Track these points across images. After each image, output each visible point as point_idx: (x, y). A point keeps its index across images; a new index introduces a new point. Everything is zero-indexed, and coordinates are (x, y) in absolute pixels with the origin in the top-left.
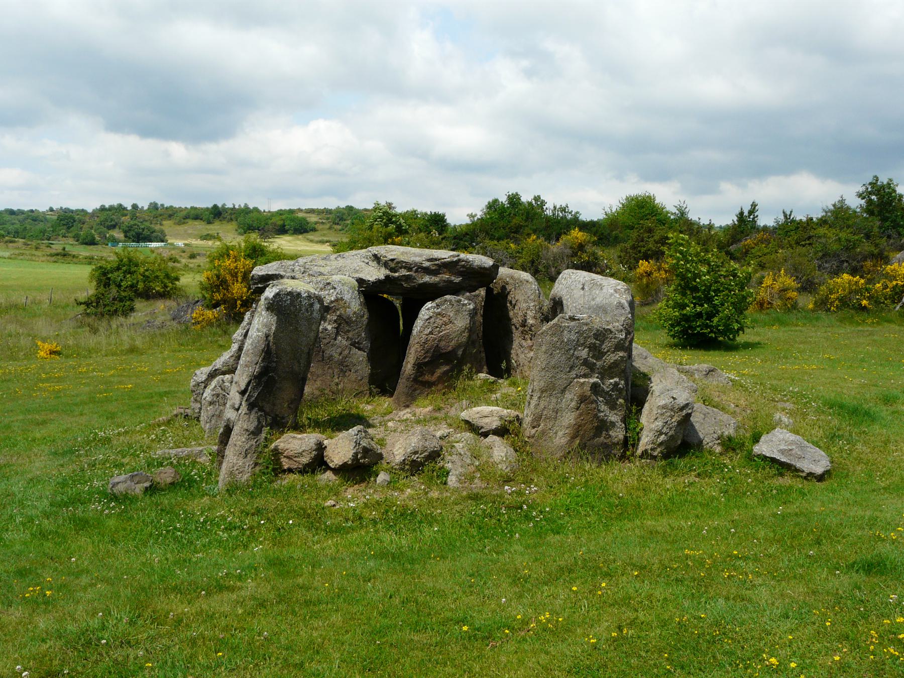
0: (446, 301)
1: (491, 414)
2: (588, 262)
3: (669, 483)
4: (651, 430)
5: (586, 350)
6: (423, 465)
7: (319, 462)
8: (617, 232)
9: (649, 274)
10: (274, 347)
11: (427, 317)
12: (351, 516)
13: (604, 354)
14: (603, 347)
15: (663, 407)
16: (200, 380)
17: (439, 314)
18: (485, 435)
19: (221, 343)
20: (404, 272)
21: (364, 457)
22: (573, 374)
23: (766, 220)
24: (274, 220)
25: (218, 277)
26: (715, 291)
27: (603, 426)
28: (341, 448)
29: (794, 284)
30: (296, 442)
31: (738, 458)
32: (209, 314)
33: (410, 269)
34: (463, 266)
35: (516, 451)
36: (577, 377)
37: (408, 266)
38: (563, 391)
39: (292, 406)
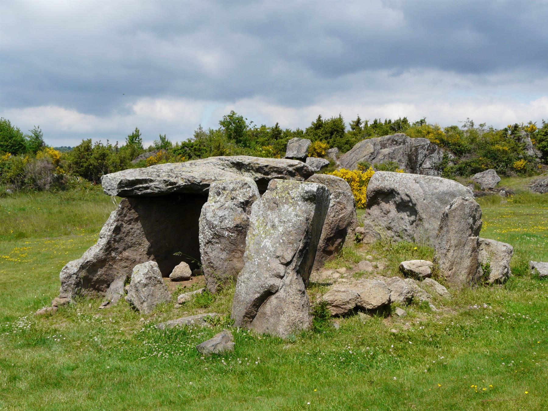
4: (501, 266)
17: (338, 202)
34: (306, 170)
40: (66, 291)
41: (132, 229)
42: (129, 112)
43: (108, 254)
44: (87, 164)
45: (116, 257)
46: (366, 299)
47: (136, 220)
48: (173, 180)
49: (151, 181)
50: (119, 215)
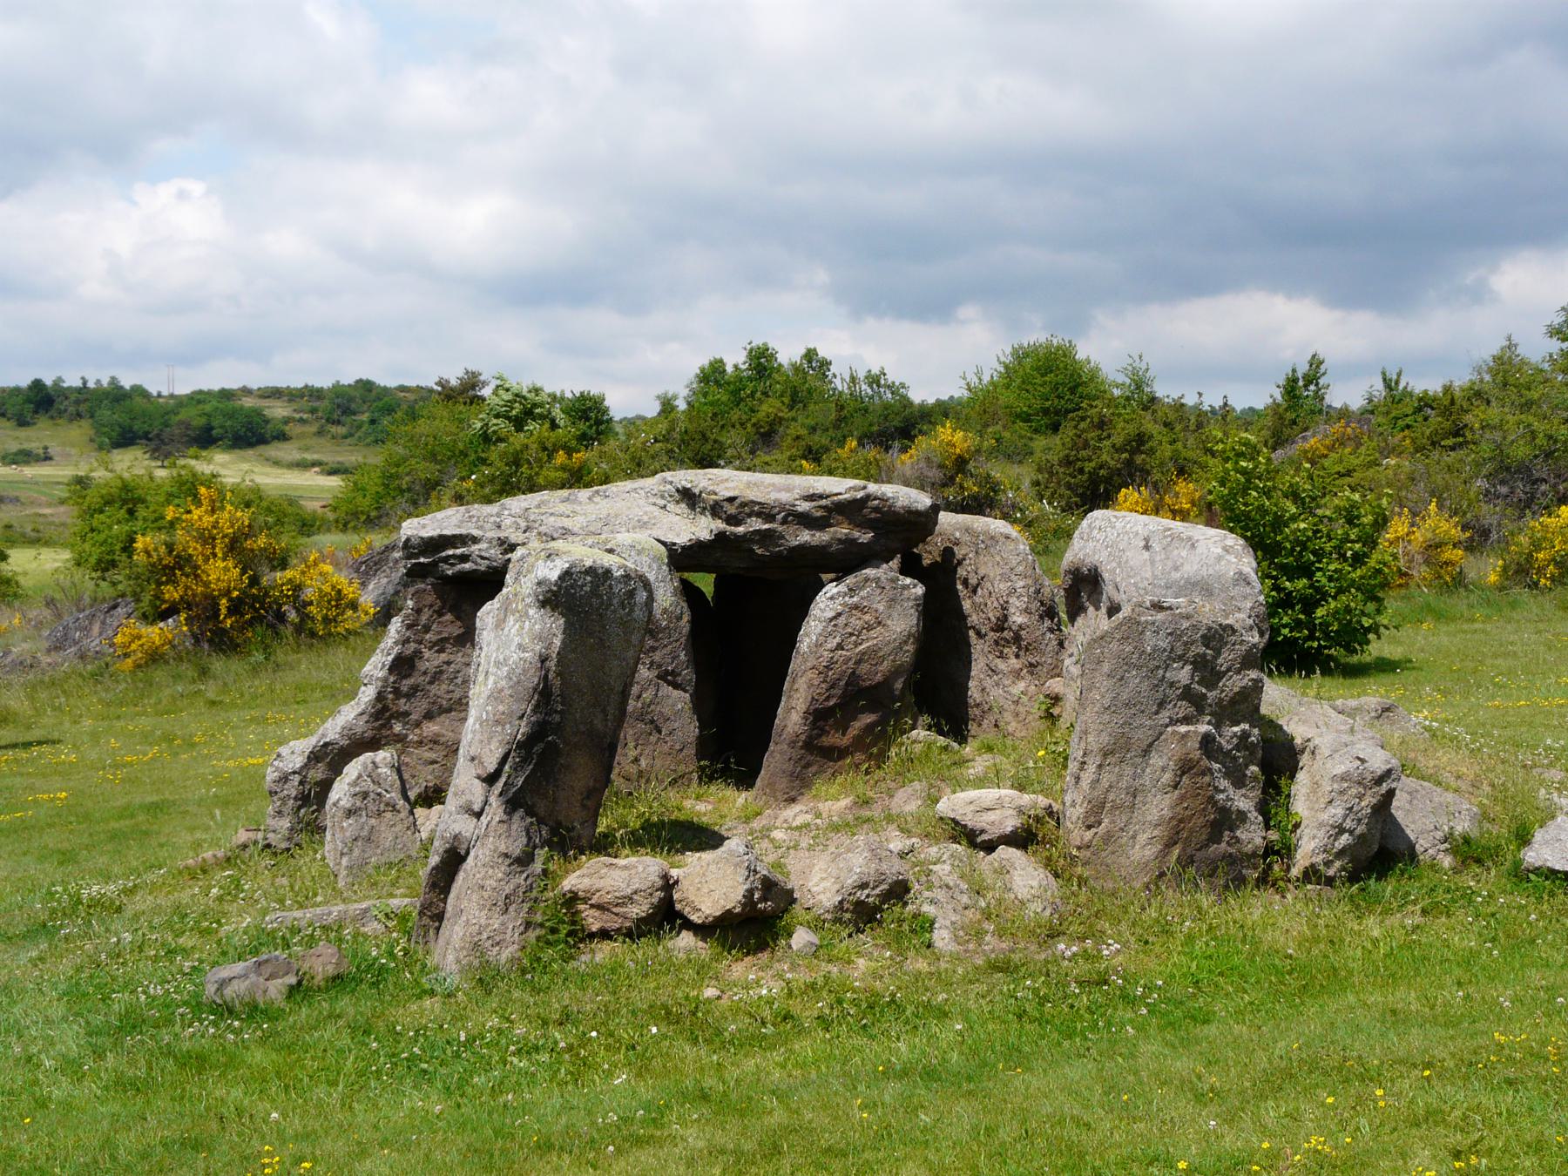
0: (867, 580)
1: (1000, 804)
2: (975, 498)
3: (1373, 926)
4: (1321, 825)
5: (1188, 668)
6: (875, 908)
7: (666, 914)
10: (557, 683)
11: (832, 614)
12: (767, 1013)
14: (1220, 661)
15: (1344, 778)
16: (289, 767)
17: (856, 607)
18: (990, 847)
19: (211, 695)
20: (756, 524)
21: (764, 899)
22: (1164, 716)
23: (1347, 393)
24: (183, 415)
25: (170, 547)
26: (1314, 553)
27: (1226, 820)
28: (711, 884)
29: (1456, 533)
30: (616, 874)
32: (155, 633)
33: (770, 518)
34: (876, 509)
35: (1056, 876)
36: (1173, 722)
38: (1146, 752)
39: (589, 803)
40: (279, 812)
41: (448, 663)
42: (1479, 295)
43: (383, 726)
44: (1093, 464)
45: (406, 736)
49: (475, 540)
50: (409, 627)
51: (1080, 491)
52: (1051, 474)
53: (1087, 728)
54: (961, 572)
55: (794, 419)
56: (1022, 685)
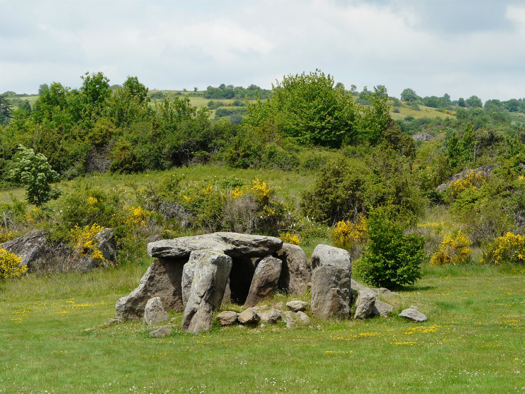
1: (298, 303)
6: (275, 321)
7: (237, 322)
8: (273, 144)
9: (346, 234)
13: (341, 279)
15: (364, 298)
16: (122, 304)
18: (296, 311)
20: (243, 246)
22: (330, 286)
27: (341, 307)
30: (227, 314)
31: (394, 318)
33: (246, 245)
34: (269, 243)
36: (332, 287)
37: (245, 244)
38: (326, 293)
44: (333, 196)
46: (242, 318)
47: (165, 273)
48: (183, 248)
49: (171, 248)
50: (153, 269)
51: (326, 210)
52: (311, 200)
53: (315, 288)
54: (288, 257)
55: (120, 134)
56: (302, 284)
